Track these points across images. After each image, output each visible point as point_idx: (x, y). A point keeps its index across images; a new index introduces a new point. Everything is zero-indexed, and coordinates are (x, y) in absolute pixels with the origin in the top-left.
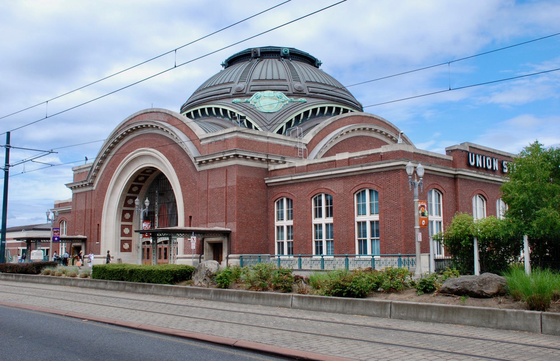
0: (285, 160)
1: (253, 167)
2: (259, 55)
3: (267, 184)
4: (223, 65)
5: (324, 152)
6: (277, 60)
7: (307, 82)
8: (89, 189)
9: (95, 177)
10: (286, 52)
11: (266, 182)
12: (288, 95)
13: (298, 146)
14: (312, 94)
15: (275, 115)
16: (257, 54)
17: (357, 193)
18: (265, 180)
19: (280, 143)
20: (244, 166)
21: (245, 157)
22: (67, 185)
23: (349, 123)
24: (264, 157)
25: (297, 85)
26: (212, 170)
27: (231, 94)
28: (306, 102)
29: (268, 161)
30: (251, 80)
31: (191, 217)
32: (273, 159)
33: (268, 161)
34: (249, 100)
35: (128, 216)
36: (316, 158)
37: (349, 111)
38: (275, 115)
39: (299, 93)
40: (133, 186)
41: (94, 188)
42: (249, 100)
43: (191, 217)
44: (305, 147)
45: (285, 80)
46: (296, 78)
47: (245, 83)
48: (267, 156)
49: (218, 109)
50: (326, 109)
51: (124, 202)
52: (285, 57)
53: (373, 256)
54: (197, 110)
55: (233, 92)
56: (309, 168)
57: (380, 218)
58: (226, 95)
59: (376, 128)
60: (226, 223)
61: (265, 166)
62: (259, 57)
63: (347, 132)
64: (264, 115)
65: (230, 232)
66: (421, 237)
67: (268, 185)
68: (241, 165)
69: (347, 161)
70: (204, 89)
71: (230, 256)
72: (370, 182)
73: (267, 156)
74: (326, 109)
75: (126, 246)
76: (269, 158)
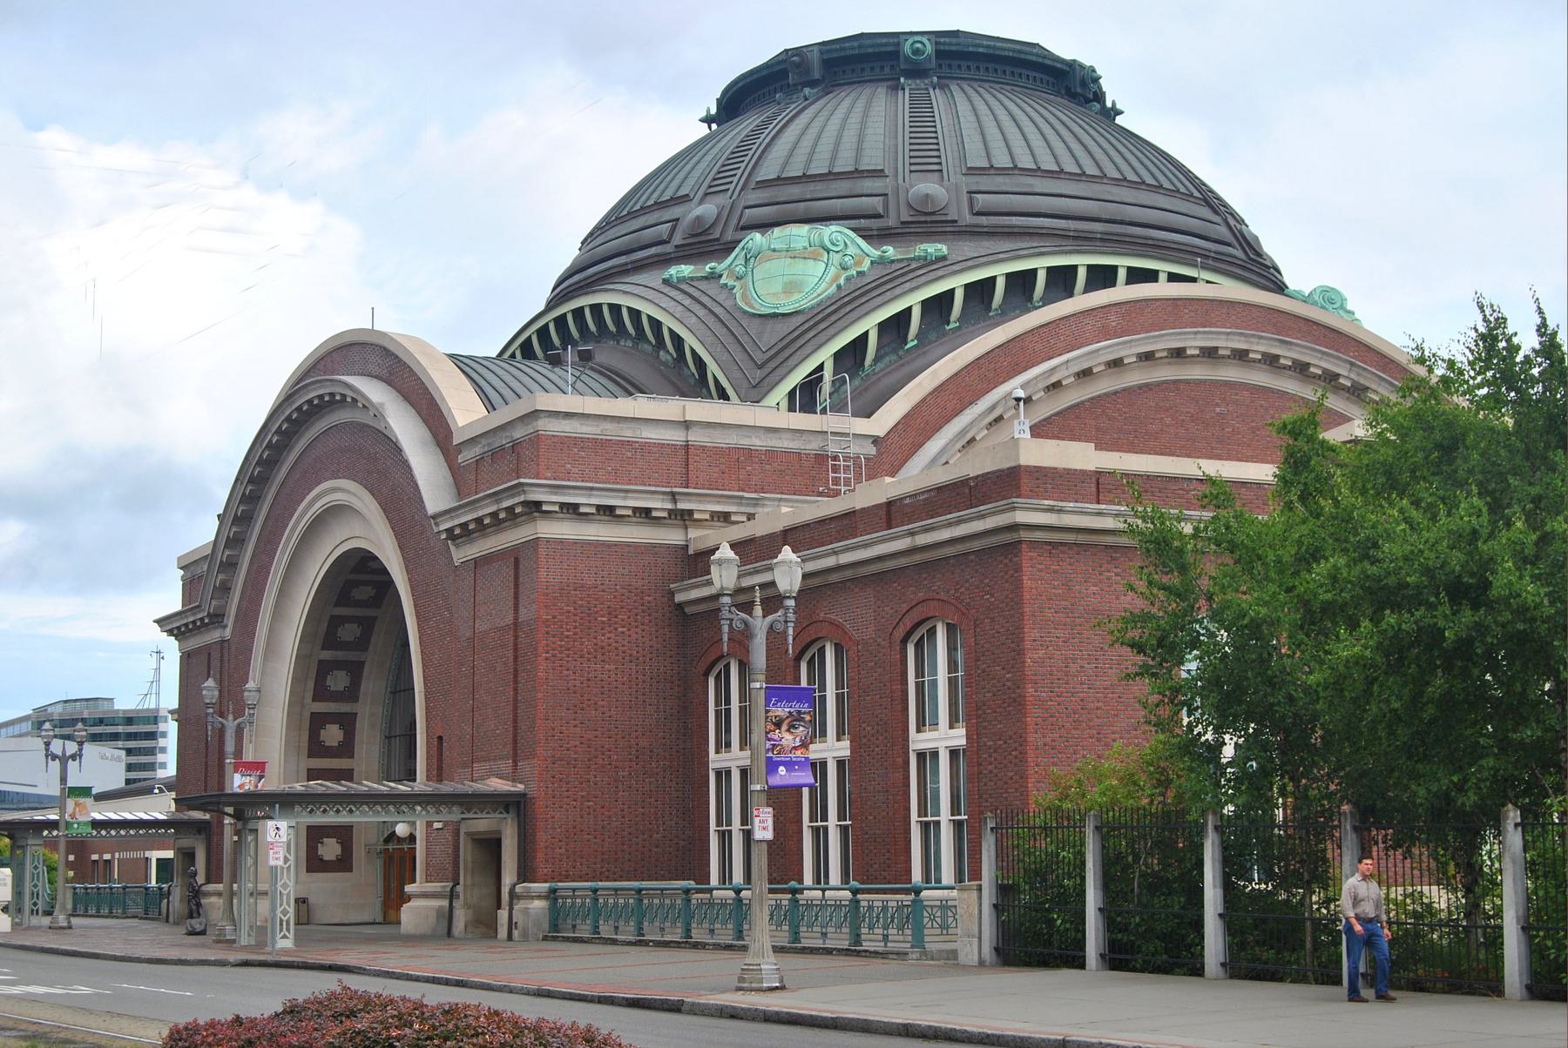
2: (817, 75)
3: (680, 606)
4: (708, 120)
6: (881, 91)
7: (973, 171)
8: (214, 636)
9: (225, 589)
10: (916, 52)
11: (679, 598)
13: (833, 448)
14: (984, 220)
15: (801, 319)
16: (808, 71)
17: (916, 637)
18: (672, 594)
20: (575, 542)
21: (608, 511)
22: (159, 622)
23: (1106, 334)
24: (659, 504)
27: (668, 248)
28: (944, 258)
29: (683, 518)
31: (440, 738)
34: (721, 267)
35: (332, 735)
37: (1163, 277)
38: (801, 319)
39: (927, 222)
40: (335, 622)
41: (228, 633)
43: (440, 738)
44: (872, 450)
45: (878, 173)
46: (926, 158)
47: (723, 200)
48: (675, 501)
49: (618, 307)
51: (311, 684)
52: (916, 71)
54: (582, 309)
55: (678, 239)
57: (968, 737)
58: (653, 251)
62: (812, 84)
64: (753, 327)
65: (524, 795)
66: (770, 823)
68: (561, 541)
69: (883, 513)
71: (518, 889)
72: (943, 596)
73: (675, 501)
74: (1000, 284)
75: (330, 849)
76: (681, 506)
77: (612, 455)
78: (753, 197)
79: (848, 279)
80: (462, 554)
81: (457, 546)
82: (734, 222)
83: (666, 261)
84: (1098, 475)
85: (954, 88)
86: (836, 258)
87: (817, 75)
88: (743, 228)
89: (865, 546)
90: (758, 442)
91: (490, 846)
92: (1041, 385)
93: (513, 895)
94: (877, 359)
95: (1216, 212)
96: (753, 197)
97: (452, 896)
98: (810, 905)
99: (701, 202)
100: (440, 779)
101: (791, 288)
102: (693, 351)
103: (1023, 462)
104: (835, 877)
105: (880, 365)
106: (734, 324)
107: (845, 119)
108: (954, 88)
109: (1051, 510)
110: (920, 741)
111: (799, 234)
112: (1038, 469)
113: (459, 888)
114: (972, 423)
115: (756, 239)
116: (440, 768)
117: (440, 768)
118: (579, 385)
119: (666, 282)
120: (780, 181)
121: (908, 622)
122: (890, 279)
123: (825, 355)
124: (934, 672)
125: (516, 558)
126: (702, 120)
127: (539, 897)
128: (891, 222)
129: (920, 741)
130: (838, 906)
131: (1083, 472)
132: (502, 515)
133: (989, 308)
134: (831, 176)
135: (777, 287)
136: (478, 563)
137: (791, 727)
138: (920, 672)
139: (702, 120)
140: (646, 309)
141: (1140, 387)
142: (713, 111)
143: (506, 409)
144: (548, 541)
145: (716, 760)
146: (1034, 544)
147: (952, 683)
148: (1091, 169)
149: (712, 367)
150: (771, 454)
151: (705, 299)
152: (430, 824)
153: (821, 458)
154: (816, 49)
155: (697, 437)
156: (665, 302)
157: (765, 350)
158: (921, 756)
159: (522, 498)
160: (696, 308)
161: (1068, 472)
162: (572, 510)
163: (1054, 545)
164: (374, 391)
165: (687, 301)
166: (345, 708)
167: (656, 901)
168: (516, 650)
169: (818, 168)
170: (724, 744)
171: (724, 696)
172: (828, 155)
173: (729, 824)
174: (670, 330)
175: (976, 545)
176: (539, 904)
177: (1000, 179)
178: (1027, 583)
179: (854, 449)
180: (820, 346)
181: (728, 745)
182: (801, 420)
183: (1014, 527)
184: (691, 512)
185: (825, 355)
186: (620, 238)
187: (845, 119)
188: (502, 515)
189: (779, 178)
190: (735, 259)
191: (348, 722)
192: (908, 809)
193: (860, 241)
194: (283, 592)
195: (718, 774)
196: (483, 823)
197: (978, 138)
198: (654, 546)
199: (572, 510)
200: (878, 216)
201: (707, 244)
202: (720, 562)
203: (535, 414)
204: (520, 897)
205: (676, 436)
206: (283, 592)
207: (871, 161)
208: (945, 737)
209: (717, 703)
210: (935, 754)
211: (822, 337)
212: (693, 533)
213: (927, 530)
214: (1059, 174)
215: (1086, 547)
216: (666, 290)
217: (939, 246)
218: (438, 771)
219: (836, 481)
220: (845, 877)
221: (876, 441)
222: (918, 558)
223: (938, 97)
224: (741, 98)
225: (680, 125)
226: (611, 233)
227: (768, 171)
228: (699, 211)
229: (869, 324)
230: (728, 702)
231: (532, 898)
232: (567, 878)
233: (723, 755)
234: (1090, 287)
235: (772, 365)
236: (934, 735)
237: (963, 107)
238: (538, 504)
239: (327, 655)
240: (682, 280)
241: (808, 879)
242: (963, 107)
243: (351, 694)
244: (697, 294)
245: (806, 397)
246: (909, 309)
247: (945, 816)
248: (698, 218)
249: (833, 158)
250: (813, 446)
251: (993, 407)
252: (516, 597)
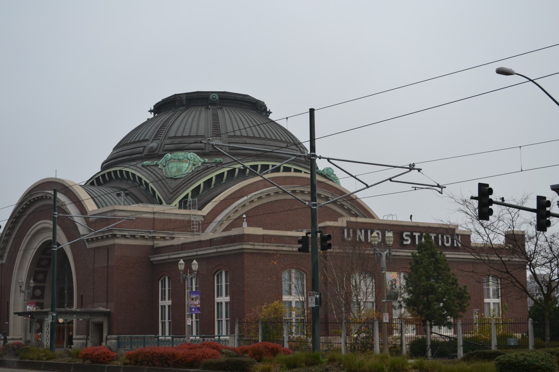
0: (173, 236)
1: (135, 245)
2: (184, 103)
3: (152, 262)
5: (226, 224)
7: (230, 136)
10: (213, 98)
12: (202, 155)
13: (192, 219)
15: (181, 180)
18: (149, 258)
19: (169, 217)
20: (125, 245)
25: (216, 142)
26: (99, 248)
27: (143, 155)
30: (167, 138)
31: (82, 296)
32: (158, 235)
33: (153, 238)
35: (38, 292)
36: (214, 231)
38: (181, 180)
41: (4, 261)
42: (159, 163)
43: (82, 296)
44: (203, 219)
46: (217, 132)
50: (100, 178)
52: (214, 103)
53: (219, 337)
54: (110, 172)
55: (145, 153)
56: (211, 242)
57: (230, 299)
58: (138, 155)
59: (302, 189)
60: (107, 304)
61: (150, 243)
62: (183, 106)
63: (269, 195)
65: (109, 312)
67: (154, 263)
68: (121, 245)
70: (127, 144)
71: (109, 337)
77: (137, 222)
78: (168, 141)
79: (195, 168)
80: (89, 246)
81: (88, 243)
82: (162, 149)
83: (142, 159)
84: (263, 235)
85: (224, 109)
86: (192, 162)
87: (184, 103)
88: (165, 151)
89: (205, 250)
90: (173, 217)
91: (99, 326)
92: (248, 201)
93: (107, 339)
94: (203, 191)
95: (297, 147)
96: (168, 141)
97: (87, 339)
98: (162, 341)
99: (152, 142)
100: (82, 307)
101: (179, 170)
102: (151, 188)
103: (245, 232)
104: (167, 334)
105: (204, 193)
106: (162, 180)
107: (193, 119)
108: (224, 109)
109: (252, 245)
110: (218, 300)
111: (181, 154)
112: (249, 234)
113: (89, 337)
114: (229, 212)
115: (169, 155)
116: (82, 304)
117: (82, 304)
118: (125, 202)
119: (143, 166)
120: (175, 137)
121: (215, 270)
122: (206, 169)
123: (189, 191)
124: (221, 282)
125: (108, 248)
126: (149, 111)
127: (114, 339)
128: (207, 151)
129: (218, 300)
130: (168, 341)
131: (259, 235)
132: (105, 237)
133: (234, 177)
134: (189, 137)
135: (174, 170)
136: (95, 249)
137: (196, 300)
138: (218, 283)
139: (149, 111)
140: (137, 174)
141: (275, 201)
142: (152, 109)
143: (107, 207)
144: (118, 244)
145: (161, 303)
146: (247, 253)
147: (226, 286)
148: (263, 136)
149: (157, 193)
150: (176, 221)
151: (154, 172)
152: (78, 320)
153: (189, 222)
154: (184, 95)
155: (156, 216)
156: (143, 173)
157: (172, 188)
158: (218, 303)
159: (111, 233)
160: (152, 175)
161: (256, 235)
162: (124, 236)
163: (252, 253)
164: (60, 196)
165: (149, 173)
166: (42, 285)
167: (136, 340)
168: (107, 273)
169: (186, 134)
170: (163, 299)
171: (164, 286)
172: (188, 130)
173: (165, 320)
174: (145, 181)
175: (233, 252)
176: (114, 341)
177: (237, 139)
178: (245, 262)
179: (198, 219)
180: (188, 188)
181: (165, 299)
182: (183, 211)
183: (243, 249)
184: (155, 237)
185: (189, 191)
186: (127, 150)
187: (193, 119)
188: (105, 237)
189: (175, 136)
190: (162, 160)
191: (42, 289)
192: (214, 317)
193: (198, 157)
194: (26, 250)
195: (162, 306)
196: (97, 319)
197: (231, 126)
198: (145, 245)
199: (124, 236)
200: (203, 149)
201: (154, 155)
202: (181, 264)
203: (114, 210)
204: (109, 339)
205: (151, 216)
206: (26, 250)
207: (201, 132)
208: (224, 299)
209: (162, 288)
210: (221, 303)
211: (189, 185)
212: (155, 242)
213: (221, 248)
214: (254, 137)
215: (260, 253)
216: (143, 168)
217: (220, 159)
218: (81, 304)
219: (193, 228)
220: (170, 334)
221: (204, 217)
222: (218, 254)
223: (219, 112)
224: (160, 108)
225: (144, 115)
226: (125, 148)
227: (172, 134)
228: (152, 145)
229: (201, 182)
230: (165, 287)
231: (112, 339)
232: (122, 334)
233: (163, 302)
234: (273, 171)
235: (175, 193)
236: (221, 298)
237: (227, 116)
238: (116, 235)
239: (37, 269)
240: (148, 166)
241: (160, 334)
242: (227, 116)
243: (44, 280)
244: (152, 171)
245: (183, 204)
246: (212, 178)
247: (224, 318)
248: (152, 147)
249: (190, 131)
250: (187, 218)
251: (235, 208)
252: (108, 258)
